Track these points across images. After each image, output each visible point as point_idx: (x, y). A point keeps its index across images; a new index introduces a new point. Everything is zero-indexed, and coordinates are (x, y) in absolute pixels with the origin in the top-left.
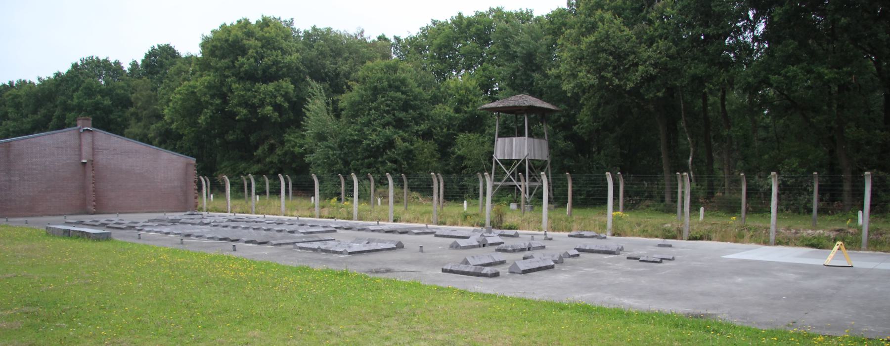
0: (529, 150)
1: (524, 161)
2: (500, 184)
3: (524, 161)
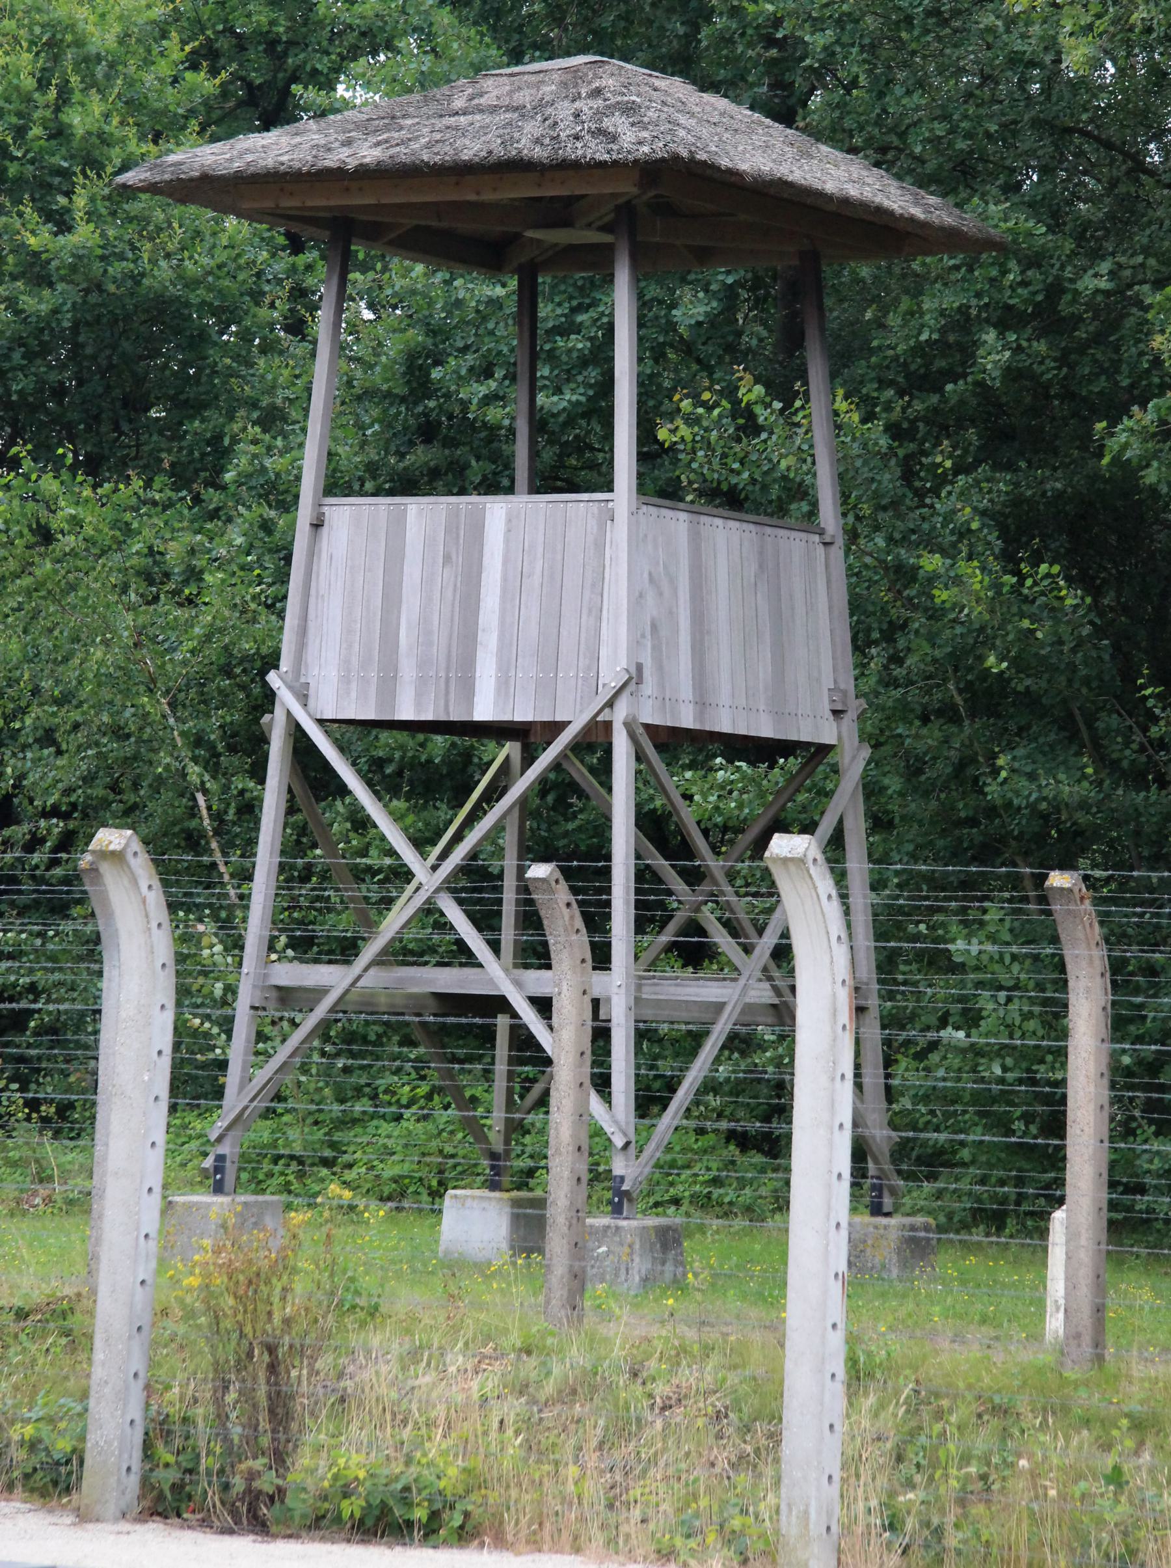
0: (652, 633)
1: (594, 744)
2: (332, 978)
3: (594, 744)
